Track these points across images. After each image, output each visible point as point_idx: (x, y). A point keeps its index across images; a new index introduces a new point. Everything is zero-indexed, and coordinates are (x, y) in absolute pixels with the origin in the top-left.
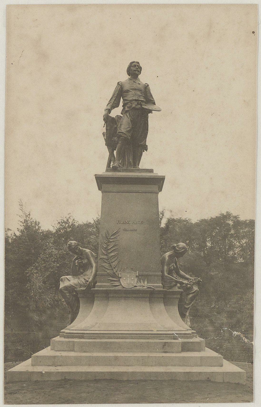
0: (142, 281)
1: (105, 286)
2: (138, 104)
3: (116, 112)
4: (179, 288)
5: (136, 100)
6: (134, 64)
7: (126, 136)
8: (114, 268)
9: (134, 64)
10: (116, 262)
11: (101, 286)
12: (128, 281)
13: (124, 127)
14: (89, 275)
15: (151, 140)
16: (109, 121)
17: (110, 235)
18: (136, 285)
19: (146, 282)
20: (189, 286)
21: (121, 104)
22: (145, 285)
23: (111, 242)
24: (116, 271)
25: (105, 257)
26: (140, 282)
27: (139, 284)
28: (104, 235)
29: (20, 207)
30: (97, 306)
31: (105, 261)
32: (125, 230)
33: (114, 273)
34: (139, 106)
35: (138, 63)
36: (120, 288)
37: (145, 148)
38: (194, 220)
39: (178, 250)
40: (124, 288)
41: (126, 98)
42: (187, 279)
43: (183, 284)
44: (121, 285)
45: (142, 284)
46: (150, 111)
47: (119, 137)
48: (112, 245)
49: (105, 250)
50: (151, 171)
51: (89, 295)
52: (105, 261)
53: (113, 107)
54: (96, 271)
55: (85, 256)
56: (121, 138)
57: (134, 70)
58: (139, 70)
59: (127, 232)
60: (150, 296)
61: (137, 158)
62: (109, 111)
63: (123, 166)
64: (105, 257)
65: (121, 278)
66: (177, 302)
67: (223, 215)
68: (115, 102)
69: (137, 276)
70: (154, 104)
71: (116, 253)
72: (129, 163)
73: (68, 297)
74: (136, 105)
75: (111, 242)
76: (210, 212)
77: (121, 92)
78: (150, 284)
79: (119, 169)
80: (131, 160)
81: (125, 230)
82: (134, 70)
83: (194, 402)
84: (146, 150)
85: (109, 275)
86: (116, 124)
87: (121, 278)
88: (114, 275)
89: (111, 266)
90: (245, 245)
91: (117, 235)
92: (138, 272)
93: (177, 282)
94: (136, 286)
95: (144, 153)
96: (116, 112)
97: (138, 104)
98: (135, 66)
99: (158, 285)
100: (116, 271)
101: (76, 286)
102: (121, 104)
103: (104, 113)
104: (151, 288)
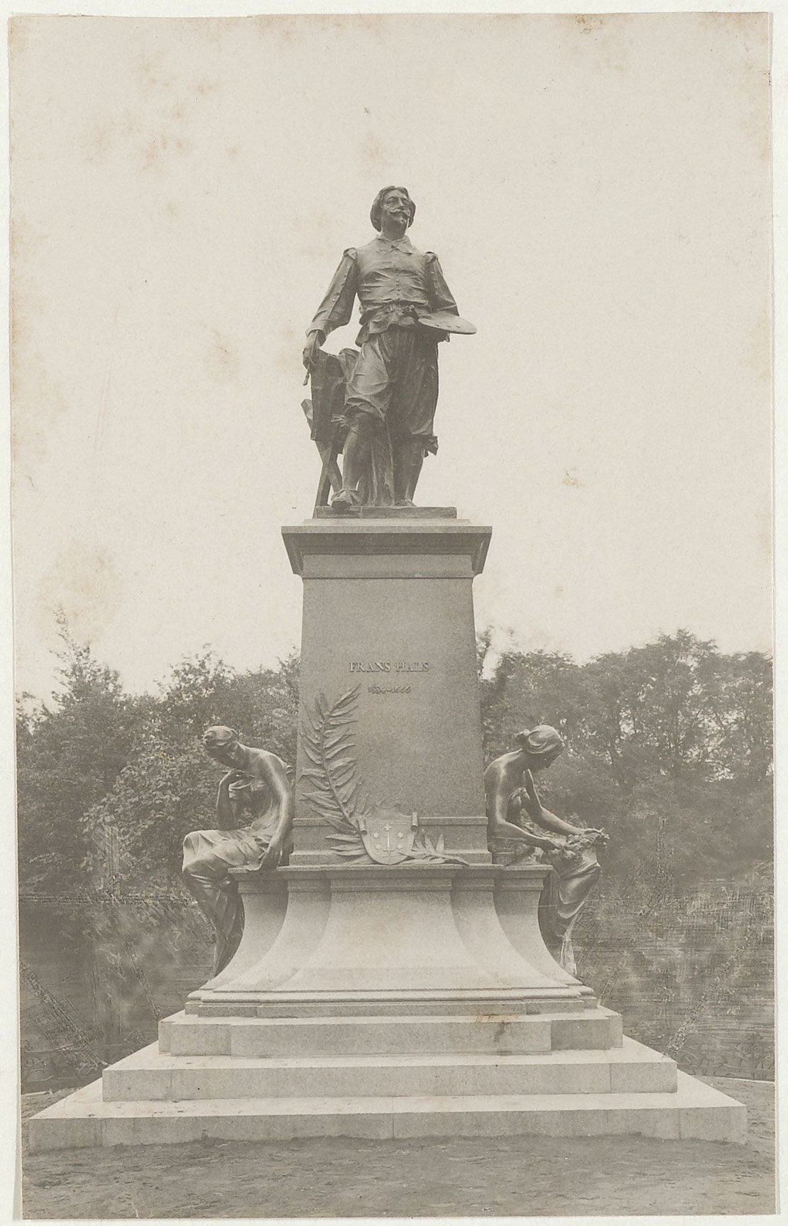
0: (427, 841)
1: (318, 859)
2: (406, 314)
3: (341, 340)
4: (540, 860)
5: (398, 303)
7: (371, 411)
12: (388, 843)
13: (367, 381)
14: (270, 828)
16: (320, 366)
17: (331, 708)
18: (412, 854)
19: (441, 846)
20: (569, 853)
21: (356, 314)
22: (437, 854)
23: (334, 727)
24: (351, 814)
27: (421, 851)
28: (312, 707)
30: (297, 919)
31: (318, 783)
34: (410, 320)
37: (430, 444)
39: (534, 748)
41: (368, 298)
44: (367, 854)
46: (443, 335)
47: (351, 413)
50: (451, 513)
51: (273, 883)
54: (291, 814)
56: (358, 415)
57: (392, 213)
58: (407, 212)
60: (454, 886)
61: (406, 478)
62: (321, 336)
63: (365, 501)
65: (365, 832)
71: (349, 759)
72: (384, 490)
73: (209, 893)
75: (334, 727)
77: (354, 281)
78: (451, 852)
80: (389, 483)
81: (375, 690)
82: (392, 213)
87: (365, 832)
88: (345, 826)
89: (334, 798)
92: (415, 815)
94: (409, 858)
95: (429, 462)
96: (341, 340)
97: (406, 314)
98: (396, 200)
99: (476, 853)
102: (356, 314)
103: (304, 342)
104: (456, 862)
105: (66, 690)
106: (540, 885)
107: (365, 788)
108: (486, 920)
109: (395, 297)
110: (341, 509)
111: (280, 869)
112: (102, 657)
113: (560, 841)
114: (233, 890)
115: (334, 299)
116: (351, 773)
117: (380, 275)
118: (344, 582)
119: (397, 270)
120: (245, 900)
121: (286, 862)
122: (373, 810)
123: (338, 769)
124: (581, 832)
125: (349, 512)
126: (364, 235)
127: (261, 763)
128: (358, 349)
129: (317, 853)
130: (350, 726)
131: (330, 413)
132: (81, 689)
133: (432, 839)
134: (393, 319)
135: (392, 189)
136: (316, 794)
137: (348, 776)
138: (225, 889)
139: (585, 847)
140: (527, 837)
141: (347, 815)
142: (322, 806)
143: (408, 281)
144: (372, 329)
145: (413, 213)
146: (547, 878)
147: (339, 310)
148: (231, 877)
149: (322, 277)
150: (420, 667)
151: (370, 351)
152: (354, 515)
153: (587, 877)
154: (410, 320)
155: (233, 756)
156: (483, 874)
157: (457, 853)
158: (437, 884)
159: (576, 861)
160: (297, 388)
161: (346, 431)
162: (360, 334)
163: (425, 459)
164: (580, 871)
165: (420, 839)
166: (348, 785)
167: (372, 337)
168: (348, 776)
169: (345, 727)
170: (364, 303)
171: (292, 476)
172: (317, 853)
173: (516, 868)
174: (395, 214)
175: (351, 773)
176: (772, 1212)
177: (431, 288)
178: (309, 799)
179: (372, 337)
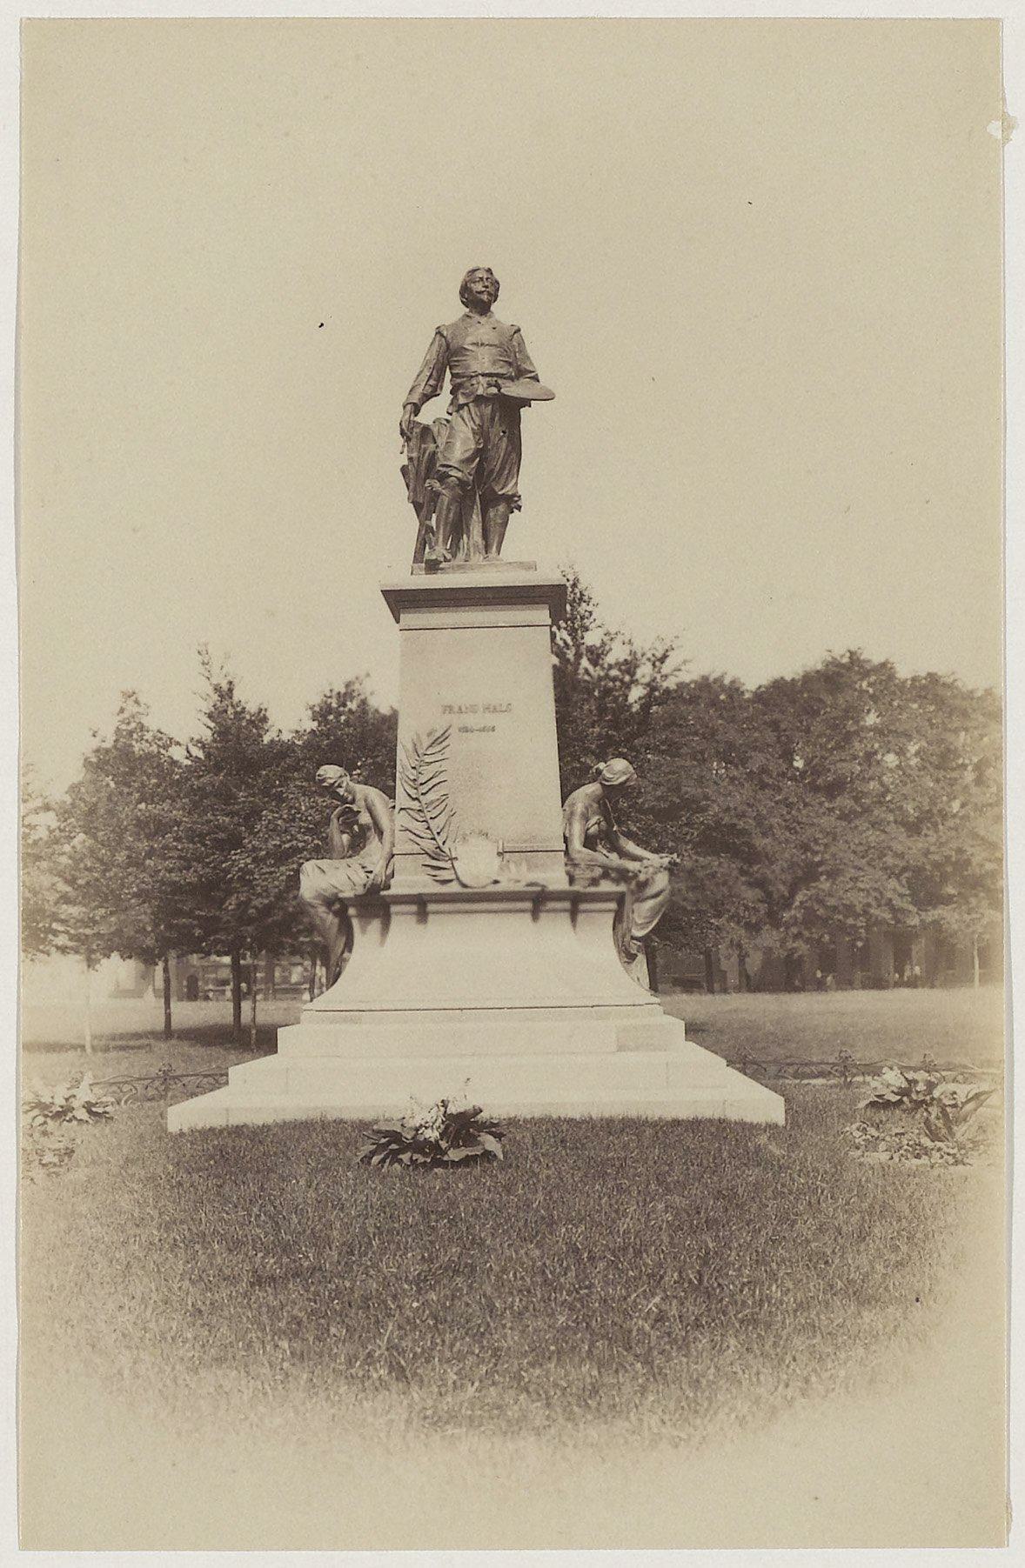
3: (435, 411)
9: (479, 274)
10: (442, 819)
13: (460, 445)
14: (374, 854)
15: (528, 481)
16: (416, 434)
19: (524, 867)
21: (447, 386)
22: (517, 877)
28: (410, 746)
29: (202, 669)
32: (465, 730)
34: (494, 390)
35: (489, 271)
36: (454, 888)
38: (753, 678)
40: (465, 886)
50: (532, 567)
51: (375, 903)
57: (479, 296)
59: (469, 735)
61: (492, 538)
62: (416, 409)
63: (454, 556)
64: (415, 805)
67: (835, 663)
76: (791, 659)
77: (448, 357)
81: (465, 730)
82: (479, 296)
83: (29, 1335)
94: (496, 882)
96: (435, 411)
99: (555, 877)
102: (447, 386)
103: (397, 414)
105: (207, 735)
106: (613, 906)
108: (555, 930)
110: (433, 567)
111: (383, 893)
112: (249, 697)
121: (388, 887)
124: (655, 860)
131: (423, 474)
132: (222, 733)
138: (336, 914)
143: (494, 350)
144: (462, 400)
146: (620, 899)
147: (432, 382)
148: (341, 900)
149: (417, 353)
153: (660, 898)
154: (494, 390)
155: (341, 791)
156: (558, 896)
158: (519, 905)
160: (396, 455)
170: (453, 375)
171: (388, 536)
173: (593, 889)
176: (1000, 1545)
177: (515, 362)
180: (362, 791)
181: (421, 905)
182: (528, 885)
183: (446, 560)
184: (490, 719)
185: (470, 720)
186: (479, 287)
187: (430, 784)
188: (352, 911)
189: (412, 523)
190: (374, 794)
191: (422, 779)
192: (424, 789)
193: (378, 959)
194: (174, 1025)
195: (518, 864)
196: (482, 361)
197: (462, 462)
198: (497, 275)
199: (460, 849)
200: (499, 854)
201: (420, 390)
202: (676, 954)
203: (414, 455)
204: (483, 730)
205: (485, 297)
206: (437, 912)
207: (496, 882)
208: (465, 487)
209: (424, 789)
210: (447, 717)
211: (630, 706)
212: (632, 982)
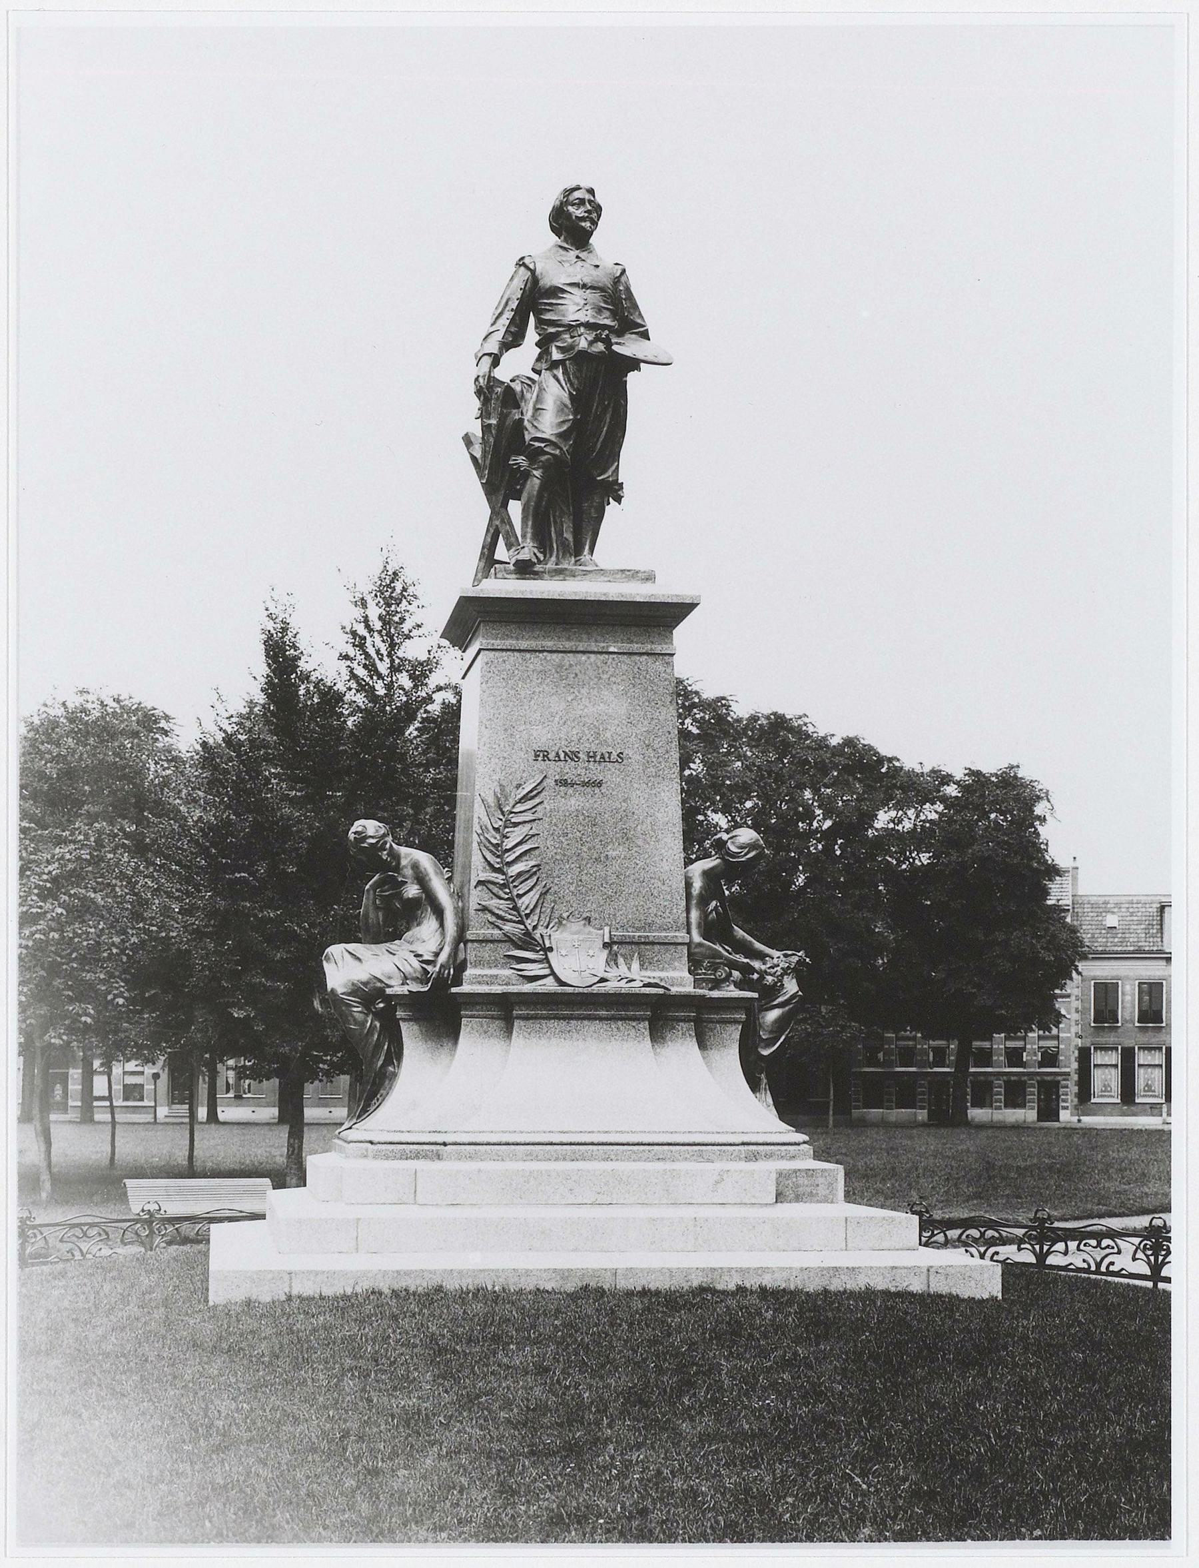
0: (621, 960)
1: (493, 979)
2: (597, 339)
4: (739, 985)
5: (588, 326)
6: (577, 194)
7: (557, 452)
8: (528, 916)
9: (577, 194)
11: (479, 980)
12: (578, 960)
13: (548, 413)
14: (427, 937)
15: (634, 462)
16: (498, 400)
17: (512, 802)
18: (606, 975)
19: (635, 965)
20: (770, 978)
21: (532, 334)
22: (631, 976)
23: (516, 825)
24: (535, 927)
25: (500, 878)
26: (616, 964)
27: (612, 973)
28: (491, 800)
30: (476, 1045)
31: (495, 890)
32: (563, 783)
33: (527, 933)
34: (600, 347)
35: (591, 191)
36: (549, 985)
37: (614, 491)
39: (735, 855)
41: (547, 316)
42: (762, 957)
43: (753, 970)
44: (553, 973)
45: (623, 970)
46: (634, 364)
47: (534, 455)
48: (516, 835)
49: (494, 854)
50: (650, 578)
51: (441, 1009)
52: (495, 890)
53: (506, 346)
54: (462, 928)
55: (408, 872)
56: (543, 458)
57: (573, 223)
58: (594, 215)
60: (657, 1014)
61: (586, 530)
62: (496, 361)
64: (500, 878)
65: (551, 949)
66: (735, 1032)
68: (513, 329)
69: (605, 945)
70: (645, 335)
71: (533, 863)
72: (563, 545)
73: (360, 1017)
74: (591, 343)
75: (516, 825)
77: (534, 299)
78: (649, 973)
79: (538, 568)
80: (568, 536)
81: (563, 783)
82: (573, 223)
84: (618, 499)
85: (508, 939)
86: (518, 407)
87: (551, 949)
88: (527, 941)
89: (515, 908)
90: (701, 818)
91: (537, 800)
92: (607, 929)
93: (733, 965)
94: (603, 980)
95: (612, 509)
96: (519, 363)
97: (597, 339)
98: (582, 202)
99: (678, 978)
100: (535, 927)
101: (390, 978)
102: (532, 334)
104: (656, 985)
107: (548, 897)
108: (682, 1050)
109: (583, 319)
113: (757, 964)
114: (390, 1010)
115: (508, 315)
116: (535, 878)
117: (563, 291)
118: (528, 655)
119: (584, 286)
120: (404, 1026)
121: (458, 981)
122: (560, 923)
123: (520, 874)
125: (536, 573)
126: (541, 242)
127: (415, 866)
128: (535, 377)
129: (494, 972)
130: (534, 825)
131: (503, 455)
133: (625, 959)
134: (583, 344)
135: (578, 188)
136: (493, 903)
137: (531, 883)
138: (378, 1015)
139: (785, 972)
140: (727, 958)
141: (530, 928)
142: (502, 918)
144: (556, 355)
145: (599, 216)
148: (388, 999)
149: (499, 286)
150: (614, 756)
151: (552, 380)
152: (537, 575)
154: (600, 347)
156: (685, 1001)
157: (653, 975)
159: (776, 989)
160: (467, 416)
161: (527, 475)
162: (539, 359)
163: (607, 508)
164: (780, 999)
165: (613, 959)
166: (531, 893)
167: (554, 365)
168: (531, 883)
169: (528, 826)
170: (540, 323)
172: (494, 972)
174: (583, 219)
175: (535, 878)
177: (619, 306)
178: (485, 909)
179: (554, 365)
180: (411, 855)
181: (506, 1011)
182: (645, 986)
183: (540, 562)
184: (596, 771)
185: (570, 770)
186: (579, 212)
187: (519, 850)
188: (400, 1014)
189: (482, 510)
190: (425, 859)
191: (508, 844)
192: (510, 857)
193: (431, 1083)
194: (198, 1164)
195: (628, 959)
196: (575, 308)
197: (559, 435)
198: (600, 199)
199: (556, 936)
200: (605, 945)
201: (499, 336)
202: (801, 1083)
203: (493, 422)
204: (585, 784)
205: (587, 225)
206: (526, 1018)
207: (603, 980)
208: (555, 461)
209: (510, 857)
210: (540, 764)
211: (941, 814)
212: (758, 1116)
